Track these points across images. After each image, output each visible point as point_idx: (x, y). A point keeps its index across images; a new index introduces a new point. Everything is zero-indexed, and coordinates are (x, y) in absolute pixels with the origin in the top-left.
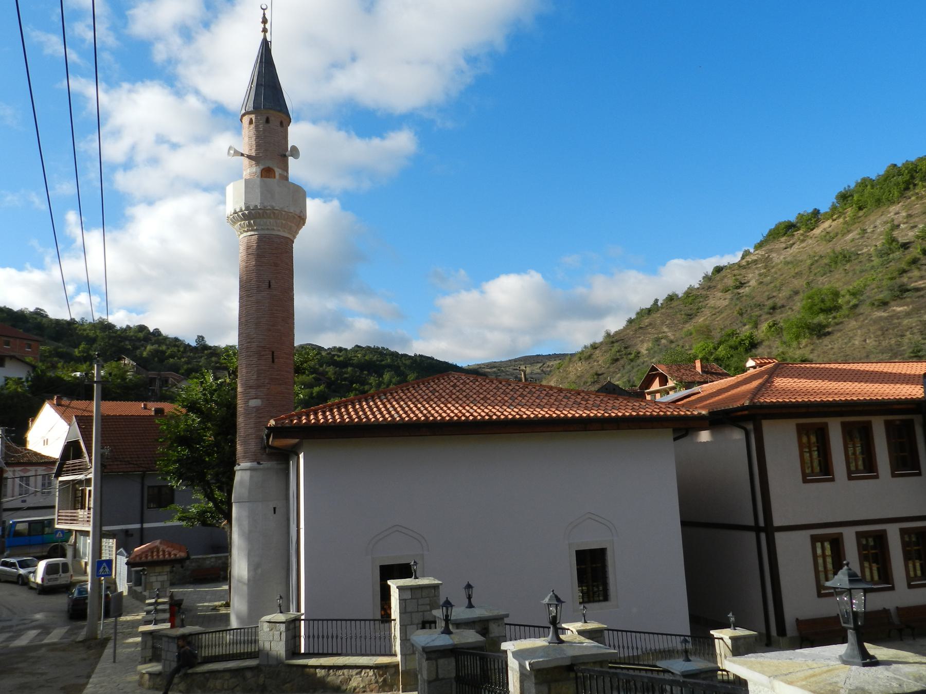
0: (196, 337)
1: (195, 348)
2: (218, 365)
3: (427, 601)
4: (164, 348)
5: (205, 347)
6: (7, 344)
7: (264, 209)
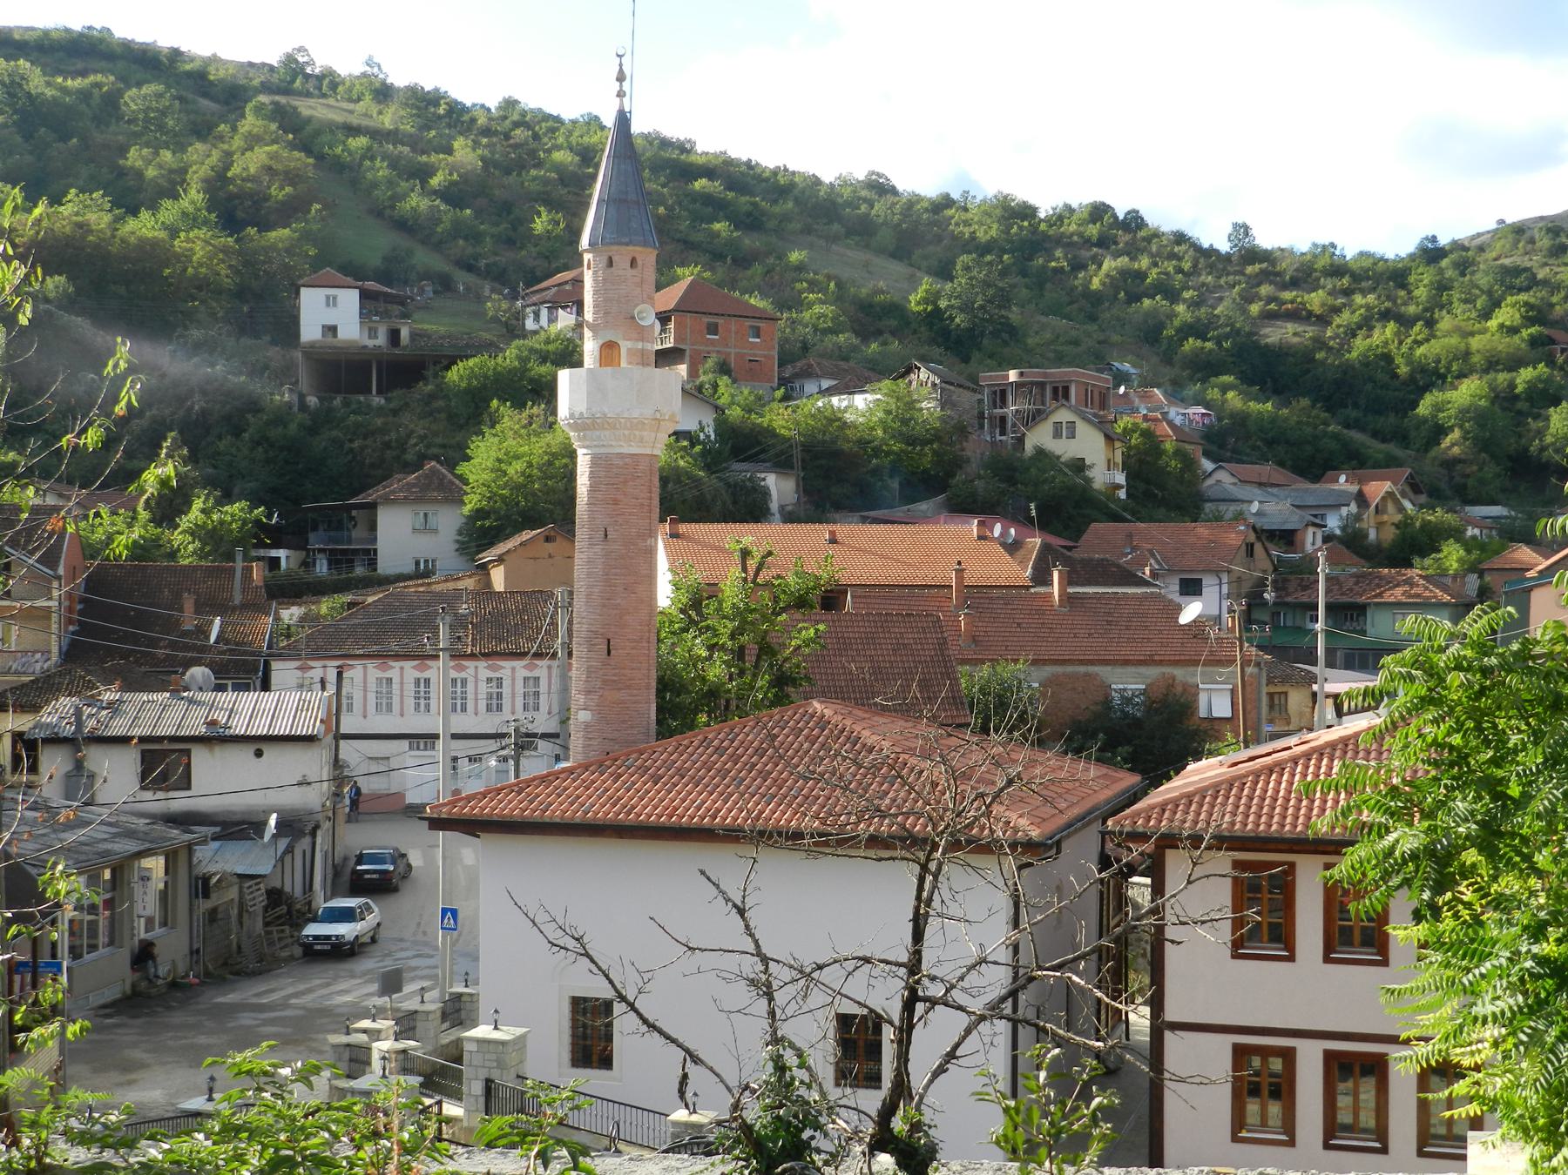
0: (1229, 229)
1: (1227, 258)
2: (1272, 306)
3: (494, 1057)
4: (1144, 262)
5: (1252, 255)
6: (713, 329)
7: (593, 417)
